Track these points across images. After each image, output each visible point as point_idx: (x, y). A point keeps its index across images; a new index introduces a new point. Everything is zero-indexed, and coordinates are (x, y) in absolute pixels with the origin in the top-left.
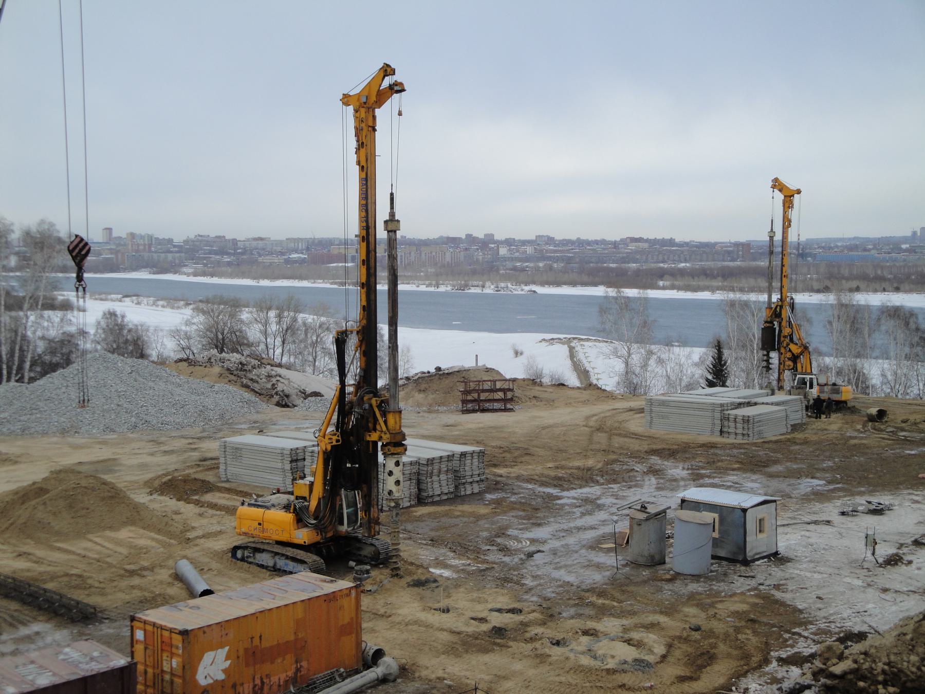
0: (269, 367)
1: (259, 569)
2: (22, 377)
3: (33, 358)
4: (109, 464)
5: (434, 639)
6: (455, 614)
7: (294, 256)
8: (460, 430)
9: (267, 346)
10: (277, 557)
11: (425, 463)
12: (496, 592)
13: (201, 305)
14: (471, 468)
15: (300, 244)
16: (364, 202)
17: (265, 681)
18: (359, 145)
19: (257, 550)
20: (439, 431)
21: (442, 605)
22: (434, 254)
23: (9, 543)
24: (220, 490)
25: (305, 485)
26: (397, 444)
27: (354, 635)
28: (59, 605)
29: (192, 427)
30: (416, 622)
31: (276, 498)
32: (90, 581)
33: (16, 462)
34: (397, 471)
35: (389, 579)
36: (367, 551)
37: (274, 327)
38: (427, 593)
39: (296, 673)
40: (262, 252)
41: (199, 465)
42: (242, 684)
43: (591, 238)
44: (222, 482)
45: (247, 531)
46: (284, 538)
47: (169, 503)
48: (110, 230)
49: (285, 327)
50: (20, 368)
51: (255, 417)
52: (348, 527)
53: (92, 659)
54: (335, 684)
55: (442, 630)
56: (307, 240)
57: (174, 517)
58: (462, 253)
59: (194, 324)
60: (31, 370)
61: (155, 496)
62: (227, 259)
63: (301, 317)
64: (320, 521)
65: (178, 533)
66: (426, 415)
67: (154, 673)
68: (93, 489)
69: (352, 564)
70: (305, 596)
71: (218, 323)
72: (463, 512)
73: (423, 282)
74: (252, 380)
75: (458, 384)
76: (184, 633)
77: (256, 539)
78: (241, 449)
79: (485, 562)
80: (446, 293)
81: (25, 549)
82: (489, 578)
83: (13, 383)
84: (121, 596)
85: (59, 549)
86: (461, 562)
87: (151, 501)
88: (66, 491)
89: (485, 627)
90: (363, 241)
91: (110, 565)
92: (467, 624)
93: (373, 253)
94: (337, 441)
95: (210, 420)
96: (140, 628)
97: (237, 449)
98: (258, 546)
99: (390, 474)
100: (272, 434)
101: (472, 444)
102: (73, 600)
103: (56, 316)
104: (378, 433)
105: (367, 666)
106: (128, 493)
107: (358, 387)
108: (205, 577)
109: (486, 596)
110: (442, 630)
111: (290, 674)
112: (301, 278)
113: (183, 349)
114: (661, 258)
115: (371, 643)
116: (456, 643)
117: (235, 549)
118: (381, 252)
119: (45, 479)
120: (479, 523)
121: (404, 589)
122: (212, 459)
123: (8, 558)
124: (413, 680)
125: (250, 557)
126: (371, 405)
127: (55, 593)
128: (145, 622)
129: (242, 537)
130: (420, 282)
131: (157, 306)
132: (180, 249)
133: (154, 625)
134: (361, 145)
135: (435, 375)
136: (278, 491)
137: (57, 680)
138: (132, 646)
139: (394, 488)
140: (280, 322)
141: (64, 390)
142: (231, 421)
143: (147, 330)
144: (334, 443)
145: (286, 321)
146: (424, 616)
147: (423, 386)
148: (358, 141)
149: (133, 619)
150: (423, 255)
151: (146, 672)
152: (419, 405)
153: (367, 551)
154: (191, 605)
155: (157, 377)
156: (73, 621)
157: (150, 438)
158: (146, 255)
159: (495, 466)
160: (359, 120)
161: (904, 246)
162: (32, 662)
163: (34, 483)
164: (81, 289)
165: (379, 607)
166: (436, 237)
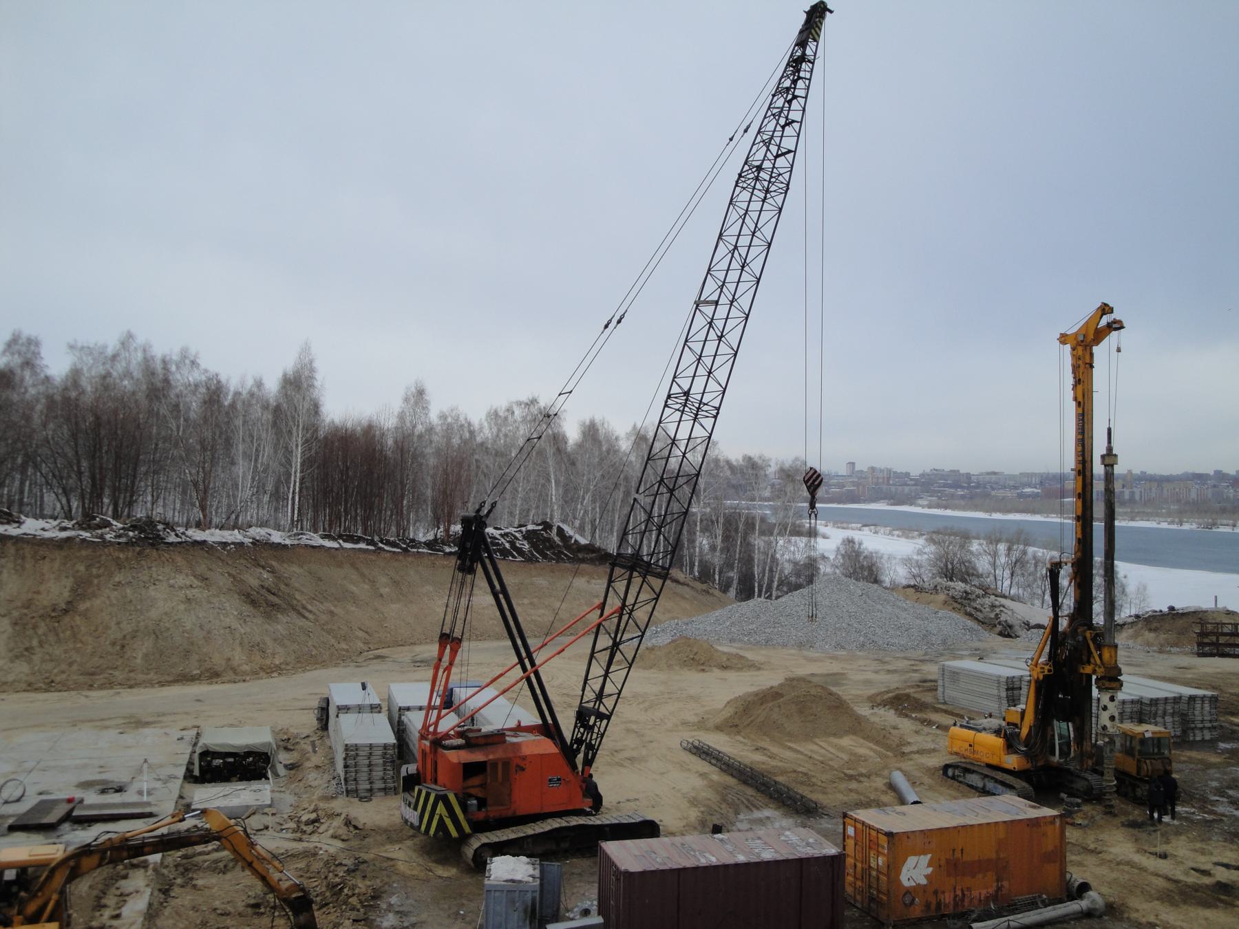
0: (993, 597)
1: (968, 788)
2: (771, 595)
3: (780, 578)
4: (837, 678)
5: (1147, 882)
6: (1173, 862)
7: (1028, 490)
8: (1194, 674)
9: (996, 579)
10: (986, 780)
11: (1148, 702)
12: (1224, 846)
13: (934, 536)
14: (1202, 713)
15: (1034, 479)
16: (1080, 437)
17: (966, 893)
18: (1076, 382)
19: (967, 771)
20: (1170, 673)
21: (1161, 848)
22: (1177, 490)
23: (749, 738)
24: (937, 710)
25: (1017, 711)
26: (1112, 679)
27: (1058, 864)
28: (786, 797)
29: (915, 650)
30: (1130, 863)
31: (988, 722)
32: (814, 780)
33: (759, 669)
34: (1111, 705)
35: (1101, 816)
36: (1080, 785)
37: (1003, 559)
38: (1144, 836)
39: (997, 891)
40: (995, 486)
41: (919, 686)
42: (943, 892)
44: (940, 703)
45: (958, 751)
46: (994, 761)
47: (888, 716)
48: (853, 464)
49: (1014, 559)
50: (769, 588)
51: (977, 644)
52: (1060, 758)
53: (808, 844)
54: (1037, 909)
55: (1157, 875)
56: (1041, 475)
57: (892, 731)
58: (1210, 490)
59: (925, 553)
60: (778, 589)
61: (876, 710)
62: (960, 492)
63: (1031, 550)
64: (1030, 749)
65: (894, 746)
66: (1156, 655)
67: (862, 869)
68: (821, 697)
69: (1064, 795)
70: (1007, 818)
71: (948, 554)
72: (1190, 758)
73: (1164, 519)
74: (976, 608)
75: (1193, 625)
76: (889, 835)
77: (968, 761)
78: (957, 673)
79: (1214, 813)
80: (1191, 531)
81: (762, 744)
82: (1216, 830)
83: (762, 599)
84: (840, 796)
85: (790, 748)
86: (1184, 809)
87: (872, 714)
88: (798, 697)
89: (1206, 880)
90: (1079, 475)
91: (832, 768)
92: (1187, 874)
93: (1090, 487)
94: (1049, 671)
95: (933, 645)
96: (852, 826)
97: (954, 672)
98: (968, 766)
99: (1105, 708)
100: (991, 661)
101: (1207, 689)
102: (798, 794)
103: (801, 542)
104: (1092, 666)
105: (1071, 898)
106: (852, 705)
107: (1072, 618)
108: (916, 789)
109: (1210, 848)
110: (1157, 875)
111: (991, 891)
112: (1034, 512)
113: (914, 576)
115: (1077, 875)
116: (1171, 891)
117: (946, 767)
118: (1099, 487)
119: (781, 685)
120: (1208, 771)
121: (1118, 828)
122: (931, 681)
123: (748, 750)
124: (1121, 920)
125: (960, 776)
126: (1085, 638)
127: (784, 785)
128: (856, 820)
129: (955, 757)
130: (1161, 519)
131: (893, 535)
132: (916, 482)
133: (863, 823)
134: (1078, 382)
135: (1168, 614)
136: (990, 716)
137: (779, 858)
138: (844, 840)
139: (1108, 723)
140: (1009, 554)
141: (802, 607)
142: (952, 647)
143: (881, 558)
144: (1046, 673)
145: (1015, 555)
146: (1138, 858)
147: (1154, 625)
148: (1075, 378)
149: (845, 816)
150: (1165, 492)
151: (855, 866)
152: (1149, 644)
153: (1080, 785)
154: (898, 811)
155: (885, 600)
156: (797, 812)
157: (876, 656)
158: (885, 487)
159: (1232, 714)
160: (1076, 358)
162: (759, 838)
163: (772, 688)
164: (813, 515)
165: (1089, 842)
166: (1180, 472)
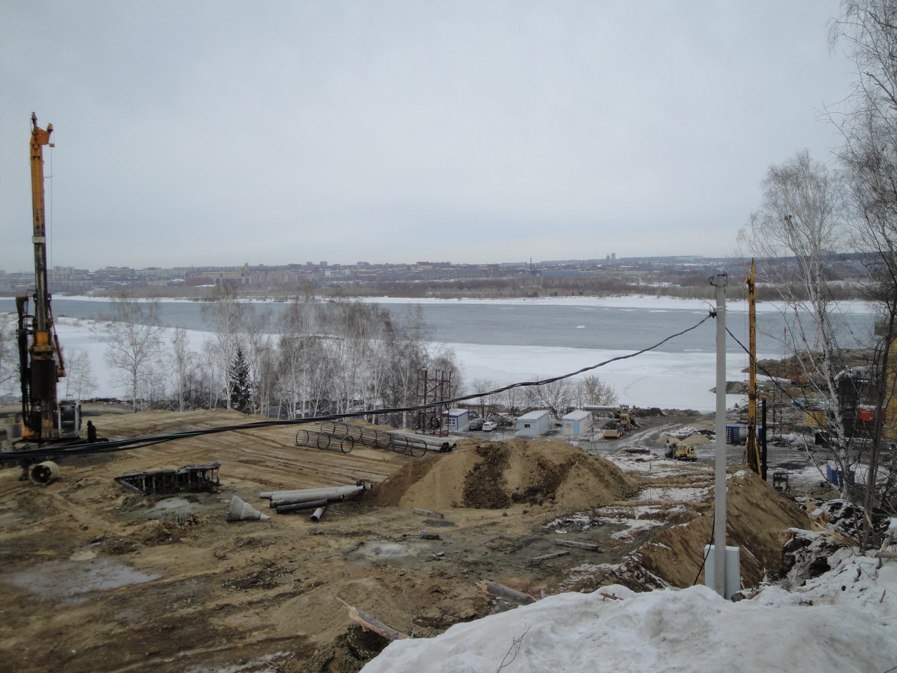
43: (395, 263)
114: (438, 275)
132: (92, 277)
161: (599, 266)
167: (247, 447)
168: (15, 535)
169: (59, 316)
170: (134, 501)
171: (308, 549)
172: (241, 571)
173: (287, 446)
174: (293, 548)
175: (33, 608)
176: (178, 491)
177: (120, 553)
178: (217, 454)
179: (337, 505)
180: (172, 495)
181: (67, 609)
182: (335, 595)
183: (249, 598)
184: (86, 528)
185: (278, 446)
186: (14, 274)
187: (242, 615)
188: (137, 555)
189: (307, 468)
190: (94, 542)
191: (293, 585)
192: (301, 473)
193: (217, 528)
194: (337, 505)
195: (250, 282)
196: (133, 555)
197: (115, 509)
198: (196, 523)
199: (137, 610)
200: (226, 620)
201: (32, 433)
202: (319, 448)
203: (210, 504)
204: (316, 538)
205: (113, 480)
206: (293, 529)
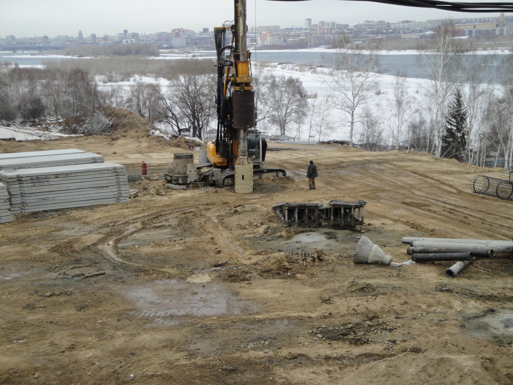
167: (419, 190)
168: (157, 249)
169: (318, 67)
170: (275, 230)
171: (424, 307)
172: (340, 319)
173: (464, 192)
174: (406, 303)
175: (127, 322)
176: (320, 225)
177: (232, 281)
178: (385, 194)
179: (486, 261)
180: (313, 229)
181: (154, 329)
182: (420, 369)
183: (328, 352)
184: (219, 252)
185: (455, 191)
186: (286, 29)
187: (311, 370)
188: (248, 285)
189: (474, 217)
190: (216, 266)
191: (385, 346)
192: (465, 222)
193: (338, 268)
194: (487, 261)
195: (505, 33)
196: (243, 284)
197: (255, 237)
198: (321, 260)
199: (213, 343)
200: (292, 373)
201: (221, 160)
202: (498, 197)
203: (347, 243)
204: (440, 294)
205: (270, 210)
206: (420, 280)
